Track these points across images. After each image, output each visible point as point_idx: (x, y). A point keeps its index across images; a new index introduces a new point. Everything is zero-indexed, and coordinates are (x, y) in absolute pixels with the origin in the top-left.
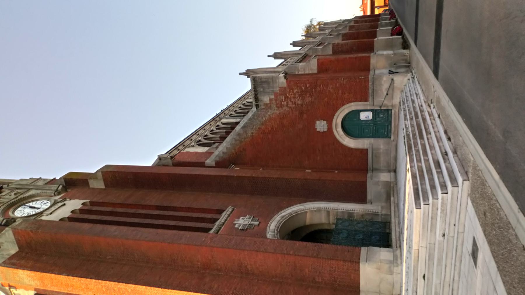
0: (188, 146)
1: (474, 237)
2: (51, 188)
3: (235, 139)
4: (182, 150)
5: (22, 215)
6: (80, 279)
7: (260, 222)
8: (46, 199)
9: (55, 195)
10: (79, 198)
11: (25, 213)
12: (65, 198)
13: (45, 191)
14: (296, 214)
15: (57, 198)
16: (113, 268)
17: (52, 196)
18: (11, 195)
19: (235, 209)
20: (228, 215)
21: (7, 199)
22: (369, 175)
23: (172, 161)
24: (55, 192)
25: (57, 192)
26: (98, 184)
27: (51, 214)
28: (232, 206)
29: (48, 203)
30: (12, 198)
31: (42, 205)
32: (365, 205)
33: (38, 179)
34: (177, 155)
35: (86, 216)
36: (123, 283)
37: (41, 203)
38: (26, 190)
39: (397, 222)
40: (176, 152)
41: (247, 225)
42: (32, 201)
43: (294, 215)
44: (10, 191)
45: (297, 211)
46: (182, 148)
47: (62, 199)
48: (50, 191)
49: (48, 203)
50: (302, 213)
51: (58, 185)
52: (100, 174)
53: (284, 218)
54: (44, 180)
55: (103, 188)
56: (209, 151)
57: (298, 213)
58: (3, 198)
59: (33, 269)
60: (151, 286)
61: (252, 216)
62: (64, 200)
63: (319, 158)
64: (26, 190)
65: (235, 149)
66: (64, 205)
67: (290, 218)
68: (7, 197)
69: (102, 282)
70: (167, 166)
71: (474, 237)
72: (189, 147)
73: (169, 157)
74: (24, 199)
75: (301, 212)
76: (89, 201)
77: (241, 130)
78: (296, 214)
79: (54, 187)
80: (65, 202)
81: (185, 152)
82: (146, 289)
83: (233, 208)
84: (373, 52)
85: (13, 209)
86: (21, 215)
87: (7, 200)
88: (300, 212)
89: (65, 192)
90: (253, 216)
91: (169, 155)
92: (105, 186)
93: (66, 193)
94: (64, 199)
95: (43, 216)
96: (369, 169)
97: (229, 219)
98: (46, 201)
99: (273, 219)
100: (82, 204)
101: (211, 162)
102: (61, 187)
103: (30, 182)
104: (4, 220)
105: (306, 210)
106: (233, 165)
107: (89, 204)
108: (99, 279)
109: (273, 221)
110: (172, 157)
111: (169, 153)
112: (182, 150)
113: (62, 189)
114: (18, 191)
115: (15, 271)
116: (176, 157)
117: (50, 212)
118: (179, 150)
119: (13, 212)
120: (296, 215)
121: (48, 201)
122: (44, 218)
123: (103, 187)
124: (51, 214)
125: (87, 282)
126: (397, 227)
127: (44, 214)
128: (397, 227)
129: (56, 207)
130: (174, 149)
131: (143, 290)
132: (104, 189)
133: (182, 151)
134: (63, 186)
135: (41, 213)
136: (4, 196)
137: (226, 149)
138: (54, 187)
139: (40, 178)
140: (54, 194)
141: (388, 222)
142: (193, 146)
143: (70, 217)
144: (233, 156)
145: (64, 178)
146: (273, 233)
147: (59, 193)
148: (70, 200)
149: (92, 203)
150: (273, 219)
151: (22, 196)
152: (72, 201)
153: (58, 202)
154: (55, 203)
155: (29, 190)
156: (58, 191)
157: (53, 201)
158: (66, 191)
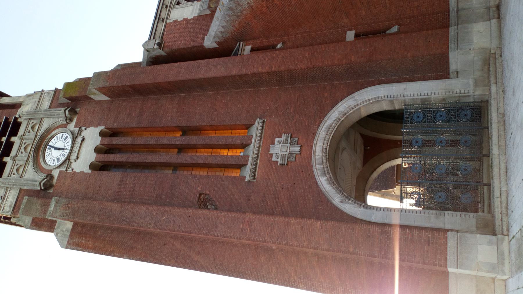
3: (227, 14)
7: (301, 146)
14: (345, 116)
19: (265, 120)
20: (259, 137)
22: (452, 31)
23: (162, 50)
25: (68, 119)
27: (78, 158)
28: (260, 118)
32: (447, 82)
34: (165, 33)
39: (503, 166)
41: (287, 155)
43: (343, 119)
45: (346, 112)
46: (167, 14)
50: (354, 112)
53: (331, 129)
56: (202, 14)
57: (347, 115)
61: (289, 135)
63: (364, 13)
65: (234, 26)
66: (83, 139)
67: (338, 126)
75: (352, 111)
77: (231, 3)
78: (345, 116)
83: (262, 121)
84: (478, 228)
88: (350, 112)
89: (76, 115)
90: (290, 135)
93: (77, 115)
96: (451, 9)
97: (263, 143)
99: (317, 138)
101: (211, 44)
105: (358, 105)
106: (242, 43)
109: (317, 141)
116: (165, 39)
120: (346, 118)
124: (78, 158)
126: (503, 183)
128: (503, 183)
137: (221, 27)
141: (484, 102)
144: (236, 33)
146: (322, 166)
147: (71, 120)
150: (317, 138)
158: (76, 113)
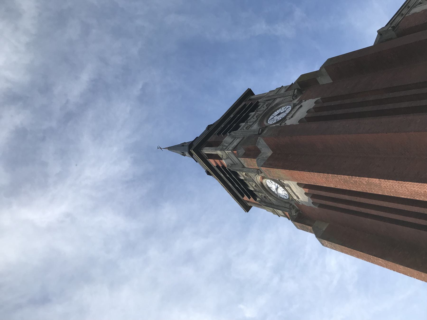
0: (414, 6)
1: (170, 148)
2: (289, 94)
4: (406, 14)
5: (272, 122)
6: (319, 174)
8: (288, 104)
9: (294, 100)
10: (312, 98)
11: (274, 120)
12: (301, 100)
13: (286, 98)
15: (295, 101)
16: (345, 162)
17: (291, 101)
18: (264, 107)
21: (262, 111)
24: (293, 96)
26: (326, 80)
29: (289, 107)
30: (265, 110)
31: (285, 109)
33: (280, 88)
35: (325, 113)
36: (356, 176)
37: (284, 109)
38: (273, 100)
40: (399, 19)
42: (278, 109)
44: (264, 103)
47: (298, 102)
48: (289, 97)
49: (289, 107)
51: (294, 90)
52: (324, 70)
54: (286, 87)
55: (330, 82)
58: (259, 111)
59: (348, 195)
60: (385, 179)
62: (300, 102)
64: (273, 100)
66: (301, 106)
68: (262, 109)
69: (338, 176)
70: (391, 39)
71: (170, 148)
72: (415, 7)
73: (390, 28)
74: (272, 108)
76: (320, 98)
79: (291, 93)
80: (301, 104)
81: (411, 14)
82: (380, 181)
85: (266, 119)
86: (272, 122)
87: (262, 112)
91: (390, 27)
92: (332, 80)
94: (301, 101)
95: (286, 120)
98: (288, 107)
100: (315, 103)
102: (296, 91)
103: (276, 92)
104: (260, 129)
107: (321, 101)
108: (334, 174)
110: (394, 28)
111: (390, 24)
112: (406, 14)
113: (297, 92)
114: (268, 102)
115: (272, 170)
117: (291, 115)
118: (402, 15)
119: (267, 122)
121: (290, 106)
122: (288, 122)
123: (332, 81)
124: (292, 117)
125: (325, 176)
127: (287, 118)
129: (295, 110)
130: (396, 16)
131: (378, 182)
132: (333, 82)
133: (407, 15)
134: (298, 90)
135: (285, 118)
136: (259, 109)
138: (291, 93)
139: (282, 86)
140: (293, 98)
142: (421, 3)
143: (306, 117)
145: (297, 82)
147: (296, 97)
148: (305, 101)
149: (324, 100)
151: (271, 106)
152: (307, 101)
153: (296, 105)
154: (294, 106)
155: (275, 99)
156: (295, 95)
157: (292, 105)
